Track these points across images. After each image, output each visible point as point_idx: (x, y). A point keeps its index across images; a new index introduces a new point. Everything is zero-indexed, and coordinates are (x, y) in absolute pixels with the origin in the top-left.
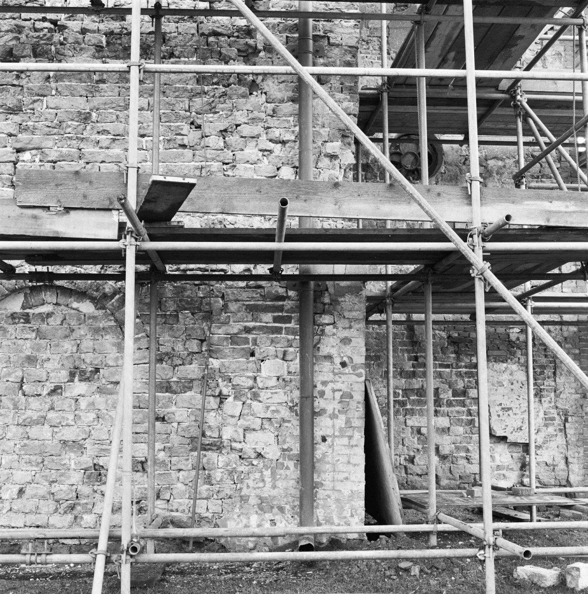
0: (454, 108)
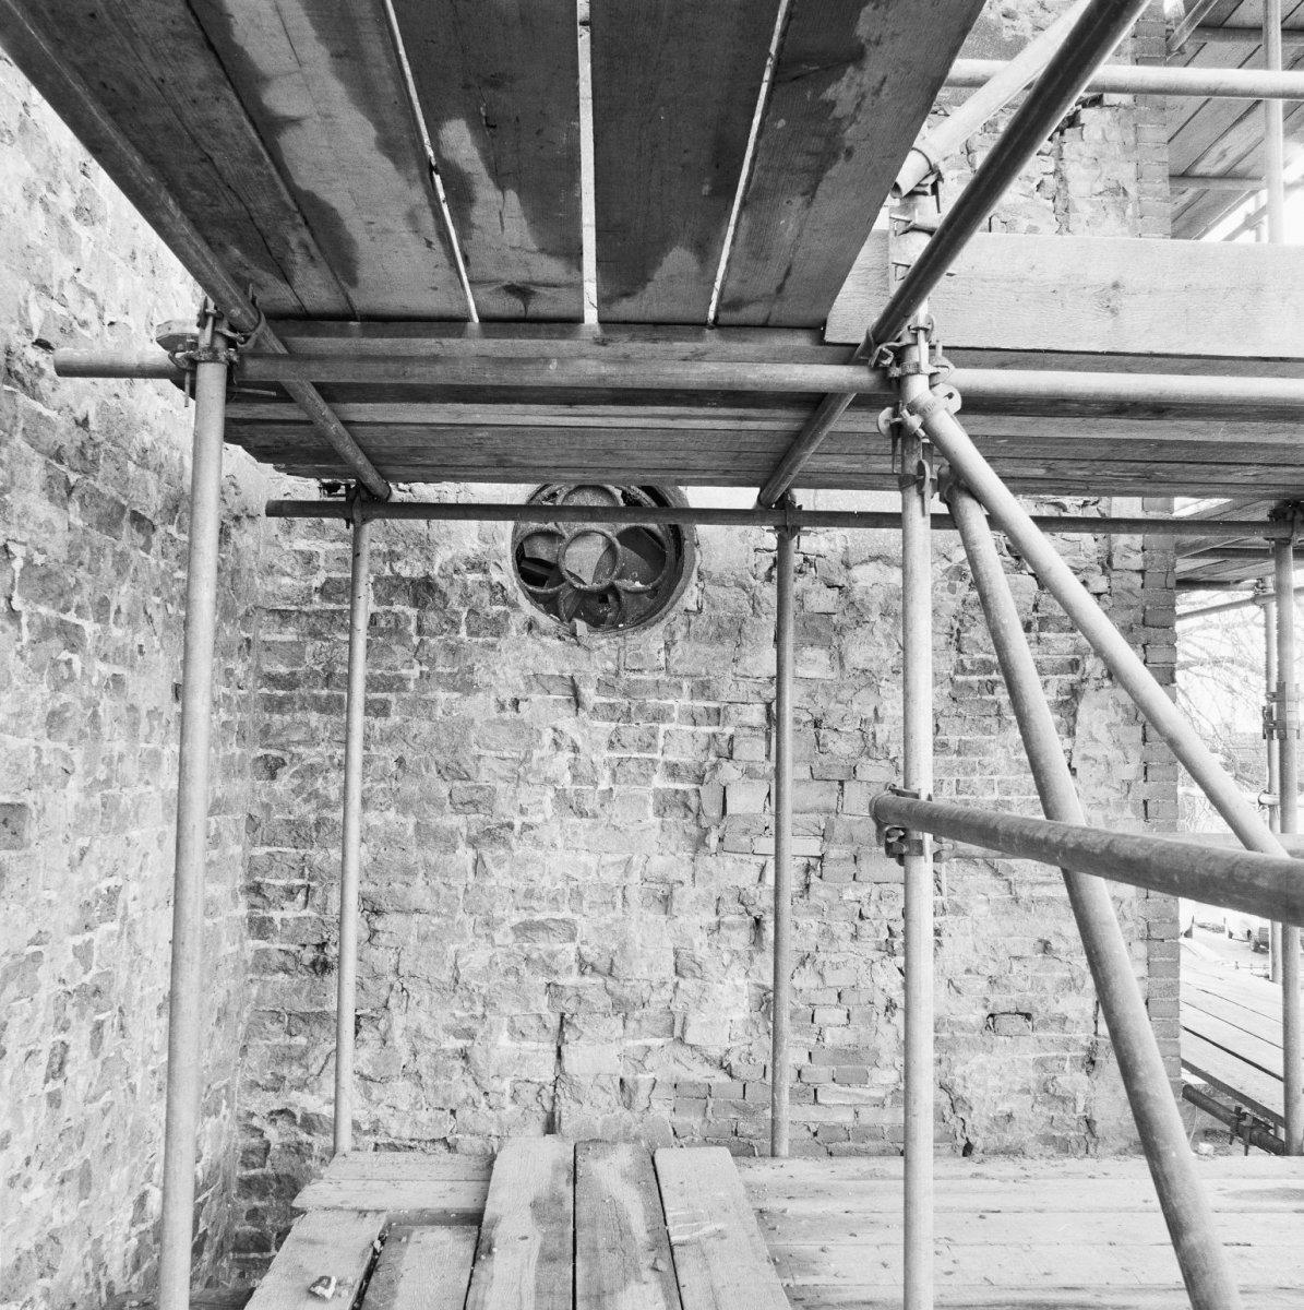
0: (650, 410)
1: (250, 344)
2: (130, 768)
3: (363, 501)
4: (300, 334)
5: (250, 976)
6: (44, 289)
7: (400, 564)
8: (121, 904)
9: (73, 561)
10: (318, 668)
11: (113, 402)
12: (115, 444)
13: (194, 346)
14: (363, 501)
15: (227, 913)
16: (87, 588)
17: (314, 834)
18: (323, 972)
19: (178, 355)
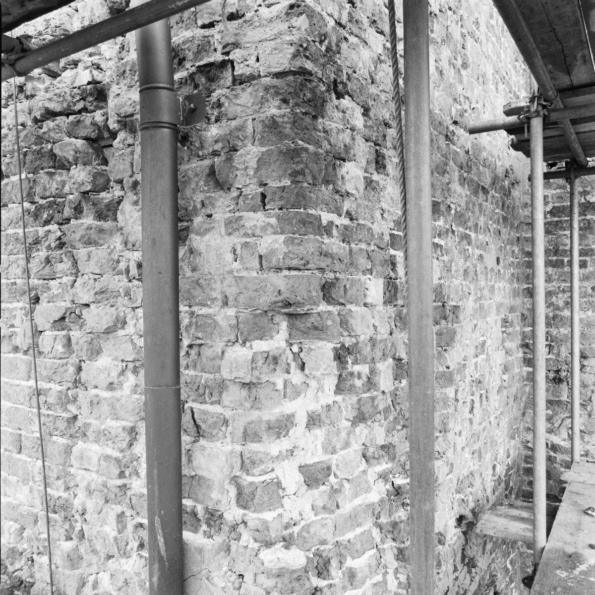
1: (553, 106)
2: (486, 292)
3: (575, 169)
4: (570, 97)
5: (525, 383)
6: (455, 100)
7: (589, 196)
8: (486, 348)
9: (468, 209)
10: (551, 248)
11: (474, 141)
12: (477, 159)
13: (529, 111)
14: (575, 169)
15: (516, 355)
16: (472, 219)
17: (552, 322)
18: (559, 383)
19: (521, 117)
